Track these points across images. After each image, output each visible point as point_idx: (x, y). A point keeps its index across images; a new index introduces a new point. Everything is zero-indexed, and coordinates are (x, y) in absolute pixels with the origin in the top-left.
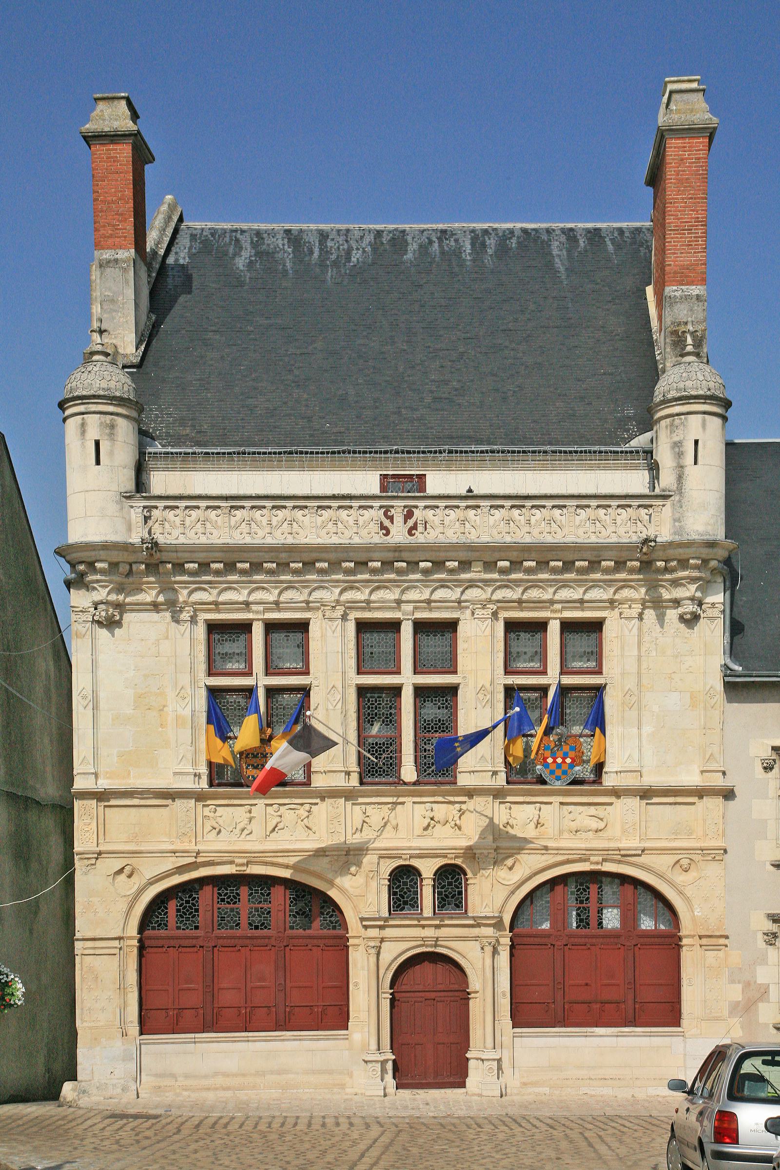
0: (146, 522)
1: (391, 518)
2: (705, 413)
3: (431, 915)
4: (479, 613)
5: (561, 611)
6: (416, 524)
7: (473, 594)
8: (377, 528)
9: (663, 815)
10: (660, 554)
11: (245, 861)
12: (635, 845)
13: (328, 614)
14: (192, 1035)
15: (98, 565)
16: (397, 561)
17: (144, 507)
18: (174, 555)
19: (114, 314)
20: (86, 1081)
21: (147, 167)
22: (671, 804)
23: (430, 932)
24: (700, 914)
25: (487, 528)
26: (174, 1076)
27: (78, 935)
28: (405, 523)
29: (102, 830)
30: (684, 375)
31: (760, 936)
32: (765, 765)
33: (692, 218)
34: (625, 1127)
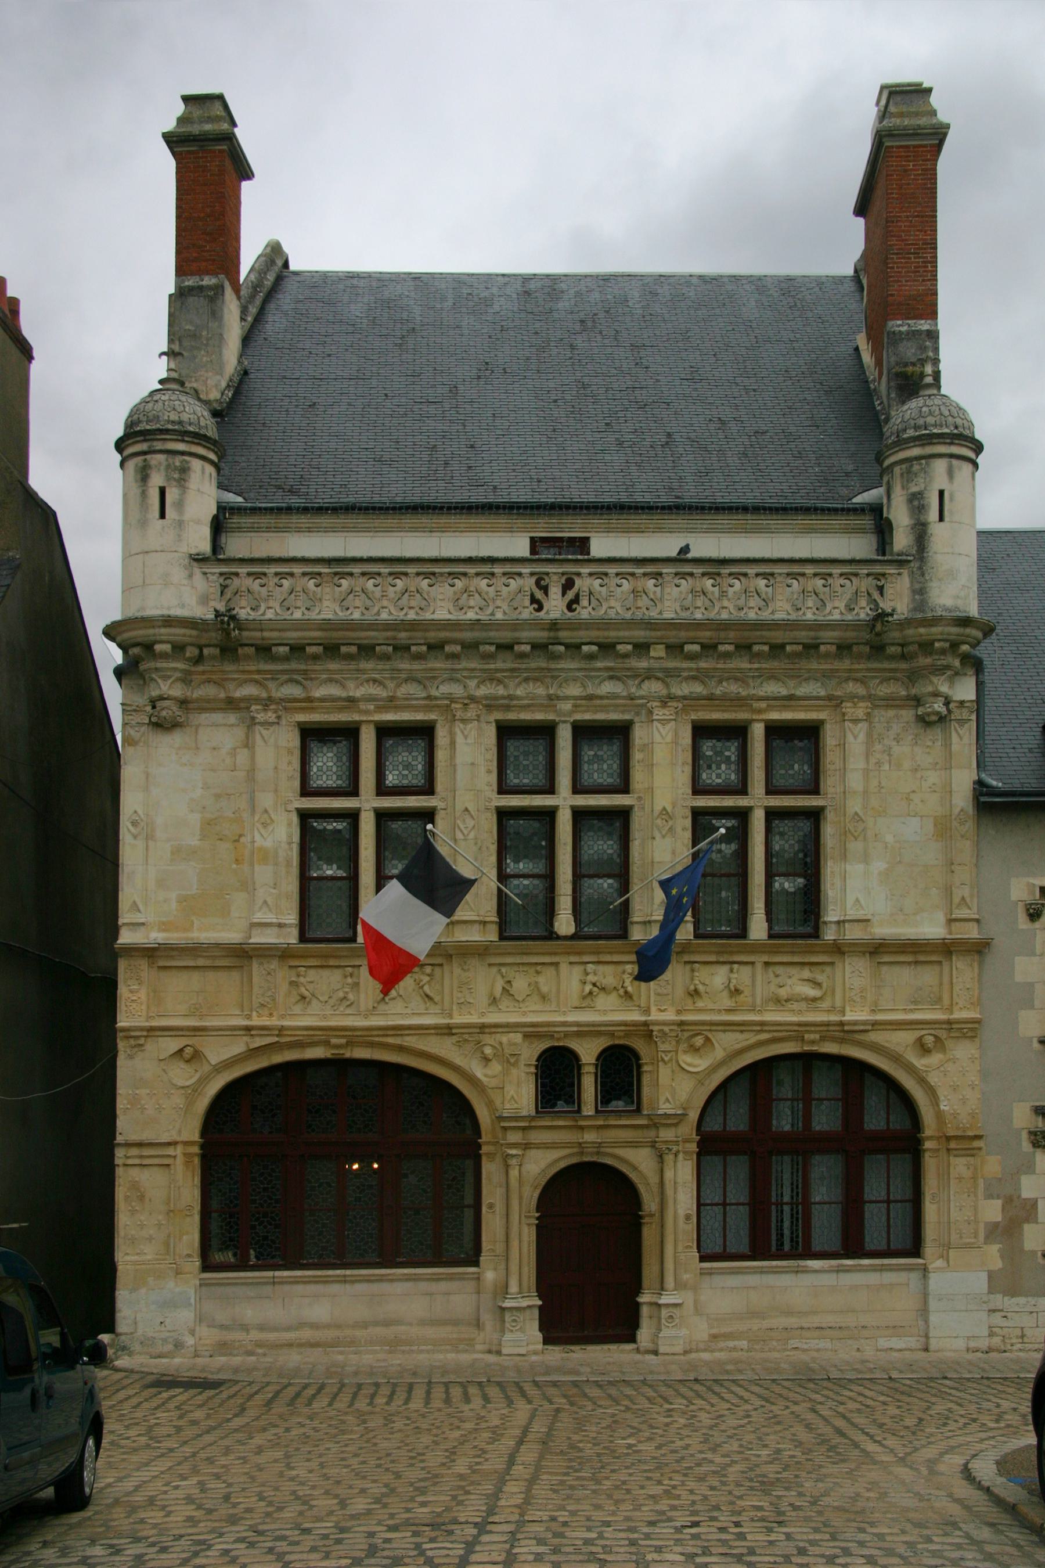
1: (545, 590)
3: (591, 1112)
5: (770, 708)
6: (577, 596)
7: (654, 687)
11: (343, 1041)
12: (863, 1018)
14: (270, 1274)
17: (221, 574)
18: (258, 634)
19: (195, 352)
20: (126, 1334)
22: (909, 963)
23: (590, 1137)
24: (946, 1108)
25: (671, 601)
26: (245, 1328)
27: (119, 1139)
31: (1024, 1135)
32: (1031, 911)
33: (919, 240)
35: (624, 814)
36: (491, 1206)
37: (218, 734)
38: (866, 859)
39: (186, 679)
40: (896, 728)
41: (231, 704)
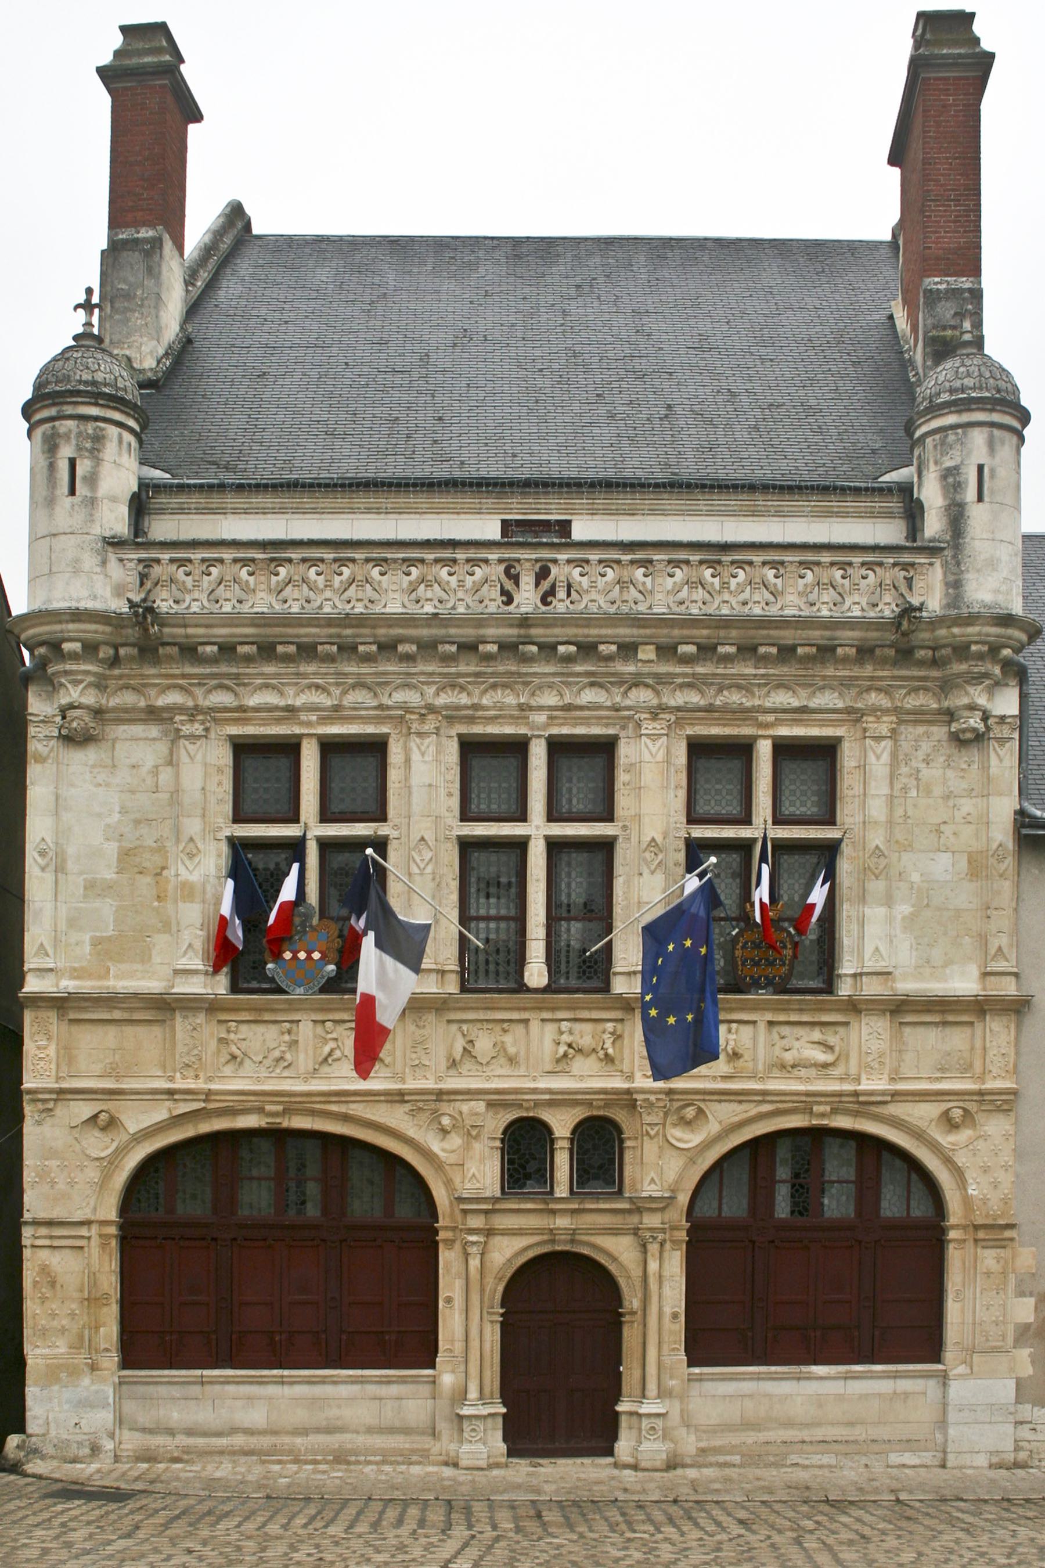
0: (142, 584)
1: (516, 579)
2: (992, 425)
3: (565, 1194)
4: (649, 727)
7: (642, 696)
8: (496, 593)
9: (928, 1042)
10: (924, 636)
13: (415, 726)
15: (67, 646)
16: (520, 646)
17: (140, 561)
21: (191, 127)
23: (562, 1222)
25: (664, 593)
27: (27, 1216)
28: (537, 585)
29: (67, 1055)
30: (961, 369)
34: (864, 1523)
35: (606, 847)
36: (449, 1300)
37: (138, 748)
38: (889, 901)
39: (100, 685)
40: (925, 747)
41: (153, 714)
